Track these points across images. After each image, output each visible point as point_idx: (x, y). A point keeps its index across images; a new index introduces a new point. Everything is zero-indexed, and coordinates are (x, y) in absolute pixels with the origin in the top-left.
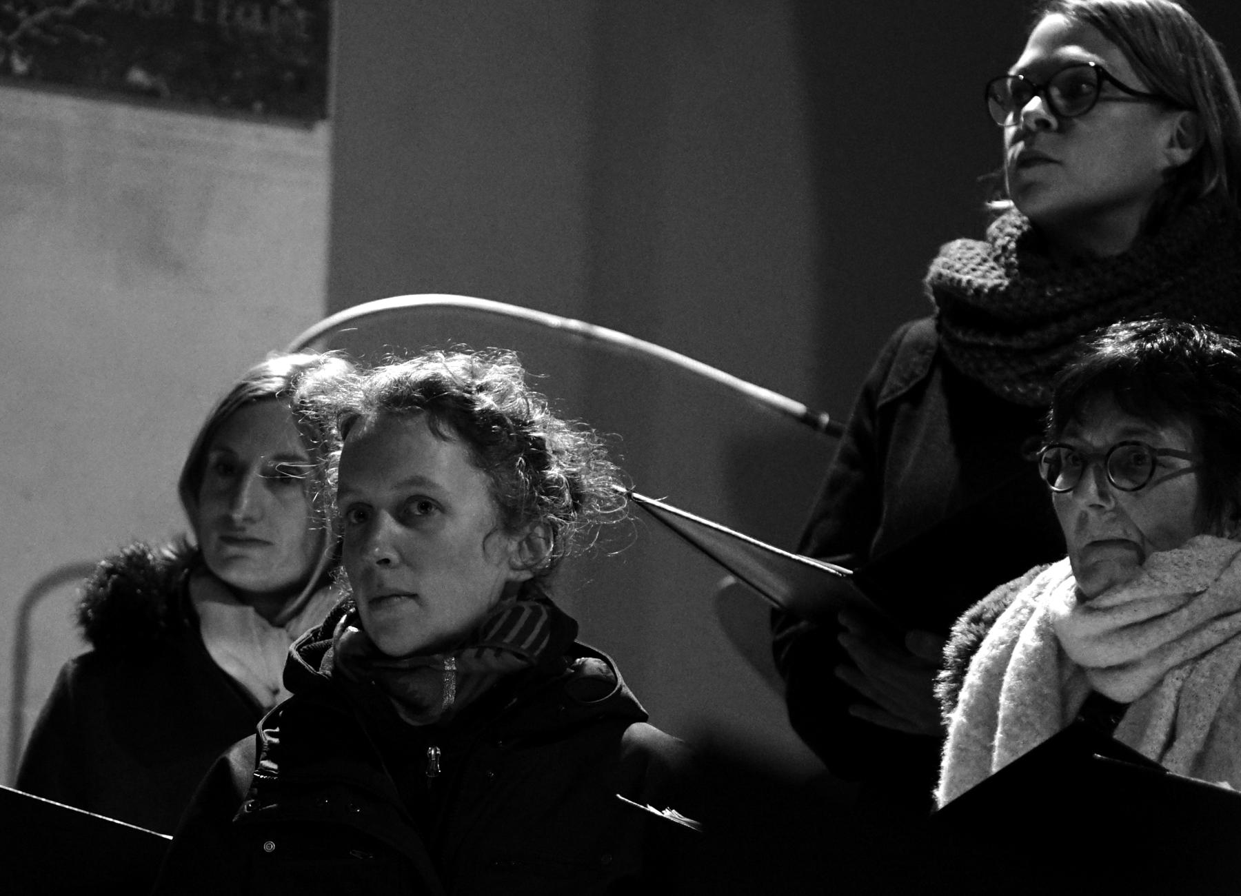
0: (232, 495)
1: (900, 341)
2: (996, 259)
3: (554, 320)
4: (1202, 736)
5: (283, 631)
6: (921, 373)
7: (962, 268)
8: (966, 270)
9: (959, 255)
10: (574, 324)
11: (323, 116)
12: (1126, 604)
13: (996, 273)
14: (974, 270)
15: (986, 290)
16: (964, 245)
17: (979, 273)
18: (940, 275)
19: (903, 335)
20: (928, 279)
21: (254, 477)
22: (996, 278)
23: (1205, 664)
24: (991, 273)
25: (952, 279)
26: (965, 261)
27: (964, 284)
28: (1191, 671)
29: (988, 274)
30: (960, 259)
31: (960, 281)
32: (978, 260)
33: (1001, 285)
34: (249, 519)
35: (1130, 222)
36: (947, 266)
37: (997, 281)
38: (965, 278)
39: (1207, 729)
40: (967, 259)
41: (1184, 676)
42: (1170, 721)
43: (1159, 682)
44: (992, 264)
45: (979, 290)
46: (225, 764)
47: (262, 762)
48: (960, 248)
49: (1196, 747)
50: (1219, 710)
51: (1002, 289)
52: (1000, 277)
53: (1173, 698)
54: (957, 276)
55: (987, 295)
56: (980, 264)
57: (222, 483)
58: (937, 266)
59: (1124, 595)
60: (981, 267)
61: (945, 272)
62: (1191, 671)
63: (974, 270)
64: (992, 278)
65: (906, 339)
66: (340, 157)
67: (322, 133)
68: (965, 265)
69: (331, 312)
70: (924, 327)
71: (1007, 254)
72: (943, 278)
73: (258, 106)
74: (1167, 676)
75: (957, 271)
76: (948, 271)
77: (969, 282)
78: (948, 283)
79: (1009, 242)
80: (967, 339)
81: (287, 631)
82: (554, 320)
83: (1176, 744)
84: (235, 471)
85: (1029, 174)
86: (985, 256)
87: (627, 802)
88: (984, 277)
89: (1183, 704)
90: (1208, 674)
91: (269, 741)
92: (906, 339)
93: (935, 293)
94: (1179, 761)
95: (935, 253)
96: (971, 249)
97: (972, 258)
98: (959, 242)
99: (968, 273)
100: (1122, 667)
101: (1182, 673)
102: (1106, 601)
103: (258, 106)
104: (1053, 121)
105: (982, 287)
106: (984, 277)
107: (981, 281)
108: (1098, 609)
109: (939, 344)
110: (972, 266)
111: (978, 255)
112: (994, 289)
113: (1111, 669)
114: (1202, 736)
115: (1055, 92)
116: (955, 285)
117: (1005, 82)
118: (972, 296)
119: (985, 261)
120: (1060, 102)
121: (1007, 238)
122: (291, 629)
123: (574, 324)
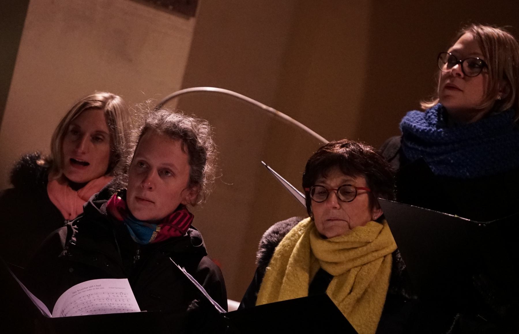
0: (78, 143)
1: (388, 144)
2: (426, 120)
3: (264, 107)
4: (361, 293)
5: (76, 192)
6: (392, 155)
7: (413, 121)
8: (414, 122)
9: (413, 116)
10: (271, 109)
11: (193, 15)
12: (345, 242)
13: (425, 124)
14: (417, 122)
15: (420, 130)
16: (415, 112)
17: (419, 123)
18: (405, 123)
19: (389, 142)
20: (401, 123)
21: (87, 138)
22: (425, 126)
23: (366, 268)
24: (423, 124)
25: (409, 125)
26: (414, 119)
27: (413, 127)
28: (361, 269)
29: (422, 124)
30: (413, 118)
31: (412, 125)
32: (419, 119)
33: (426, 129)
34: (84, 153)
35: (479, 116)
36: (408, 120)
37: (425, 128)
38: (414, 125)
39: (364, 291)
40: (416, 118)
41: (358, 270)
42: (352, 285)
43: (349, 271)
44: (424, 121)
45: (418, 130)
46: (58, 235)
47: (73, 238)
48: (413, 114)
49: (359, 296)
50: (369, 285)
51: (426, 131)
52: (427, 126)
53: (354, 278)
54: (411, 123)
55: (420, 132)
56: (420, 120)
57: (74, 137)
58: (404, 120)
59: (346, 239)
60: (420, 122)
61: (407, 122)
62: (361, 269)
63: (417, 122)
64: (422, 126)
65: (391, 143)
66: (197, 32)
67: (192, 21)
68: (414, 120)
69: (183, 88)
70: (397, 139)
71: (430, 119)
72: (406, 124)
73: (171, 7)
74: (352, 269)
75: (411, 122)
76: (408, 122)
77: (415, 126)
78: (407, 126)
79: (432, 115)
80: (411, 146)
81: (78, 192)
82: (264, 107)
83: (352, 293)
84: (79, 134)
85: (449, 92)
86: (422, 118)
87: (188, 278)
88: (421, 125)
89: (356, 280)
90: (367, 271)
91: (75, 231)
92: (391, 143)
93: (403, 128)
94: (352, 299)
95: (405, 115)
96: (418, 114)
97: (417, 118)
98: (414, 112)
99: (415, 123)
100: (336, 263)
101: (358, 269)
102: (336, 240)
103: (171, 7)
104: (462, 75)
105: (419, 128)
106: (421, 125)
107: (419, 126)
108: (333, 242)
109: (401, 147)
110: (417, 121)
111: (420, 117)
112: (423, 130)
113: (327, 262)
114: (362, 292)
115: (465, 64)
116: (410, 127)
117: (446, 55)
118: (415, 132)
119: (422, 119)
120: (467, 69)
121: (431, 113)
122: (79, 192)
123: (271, 109)
